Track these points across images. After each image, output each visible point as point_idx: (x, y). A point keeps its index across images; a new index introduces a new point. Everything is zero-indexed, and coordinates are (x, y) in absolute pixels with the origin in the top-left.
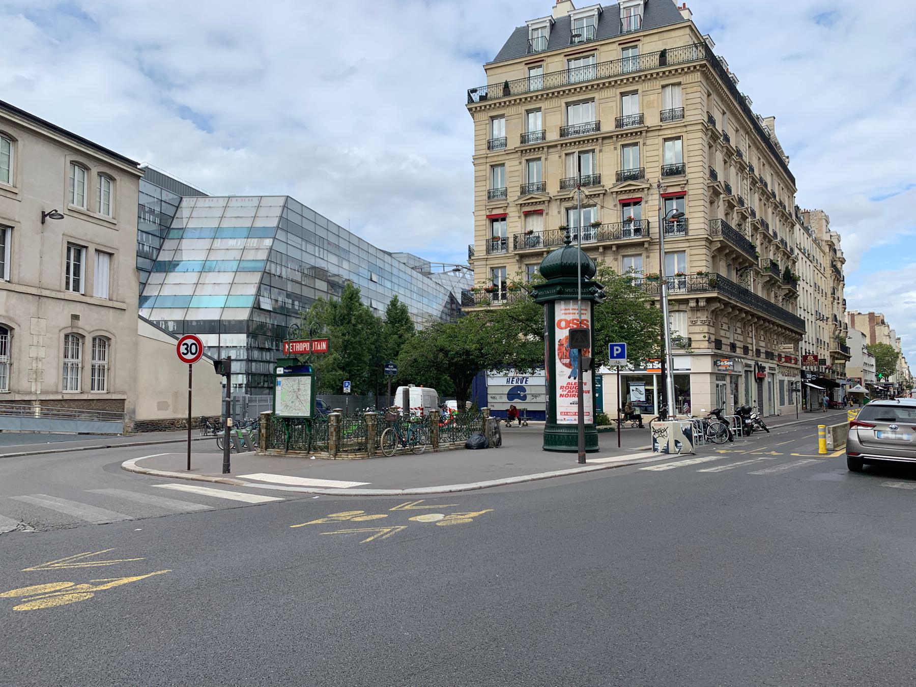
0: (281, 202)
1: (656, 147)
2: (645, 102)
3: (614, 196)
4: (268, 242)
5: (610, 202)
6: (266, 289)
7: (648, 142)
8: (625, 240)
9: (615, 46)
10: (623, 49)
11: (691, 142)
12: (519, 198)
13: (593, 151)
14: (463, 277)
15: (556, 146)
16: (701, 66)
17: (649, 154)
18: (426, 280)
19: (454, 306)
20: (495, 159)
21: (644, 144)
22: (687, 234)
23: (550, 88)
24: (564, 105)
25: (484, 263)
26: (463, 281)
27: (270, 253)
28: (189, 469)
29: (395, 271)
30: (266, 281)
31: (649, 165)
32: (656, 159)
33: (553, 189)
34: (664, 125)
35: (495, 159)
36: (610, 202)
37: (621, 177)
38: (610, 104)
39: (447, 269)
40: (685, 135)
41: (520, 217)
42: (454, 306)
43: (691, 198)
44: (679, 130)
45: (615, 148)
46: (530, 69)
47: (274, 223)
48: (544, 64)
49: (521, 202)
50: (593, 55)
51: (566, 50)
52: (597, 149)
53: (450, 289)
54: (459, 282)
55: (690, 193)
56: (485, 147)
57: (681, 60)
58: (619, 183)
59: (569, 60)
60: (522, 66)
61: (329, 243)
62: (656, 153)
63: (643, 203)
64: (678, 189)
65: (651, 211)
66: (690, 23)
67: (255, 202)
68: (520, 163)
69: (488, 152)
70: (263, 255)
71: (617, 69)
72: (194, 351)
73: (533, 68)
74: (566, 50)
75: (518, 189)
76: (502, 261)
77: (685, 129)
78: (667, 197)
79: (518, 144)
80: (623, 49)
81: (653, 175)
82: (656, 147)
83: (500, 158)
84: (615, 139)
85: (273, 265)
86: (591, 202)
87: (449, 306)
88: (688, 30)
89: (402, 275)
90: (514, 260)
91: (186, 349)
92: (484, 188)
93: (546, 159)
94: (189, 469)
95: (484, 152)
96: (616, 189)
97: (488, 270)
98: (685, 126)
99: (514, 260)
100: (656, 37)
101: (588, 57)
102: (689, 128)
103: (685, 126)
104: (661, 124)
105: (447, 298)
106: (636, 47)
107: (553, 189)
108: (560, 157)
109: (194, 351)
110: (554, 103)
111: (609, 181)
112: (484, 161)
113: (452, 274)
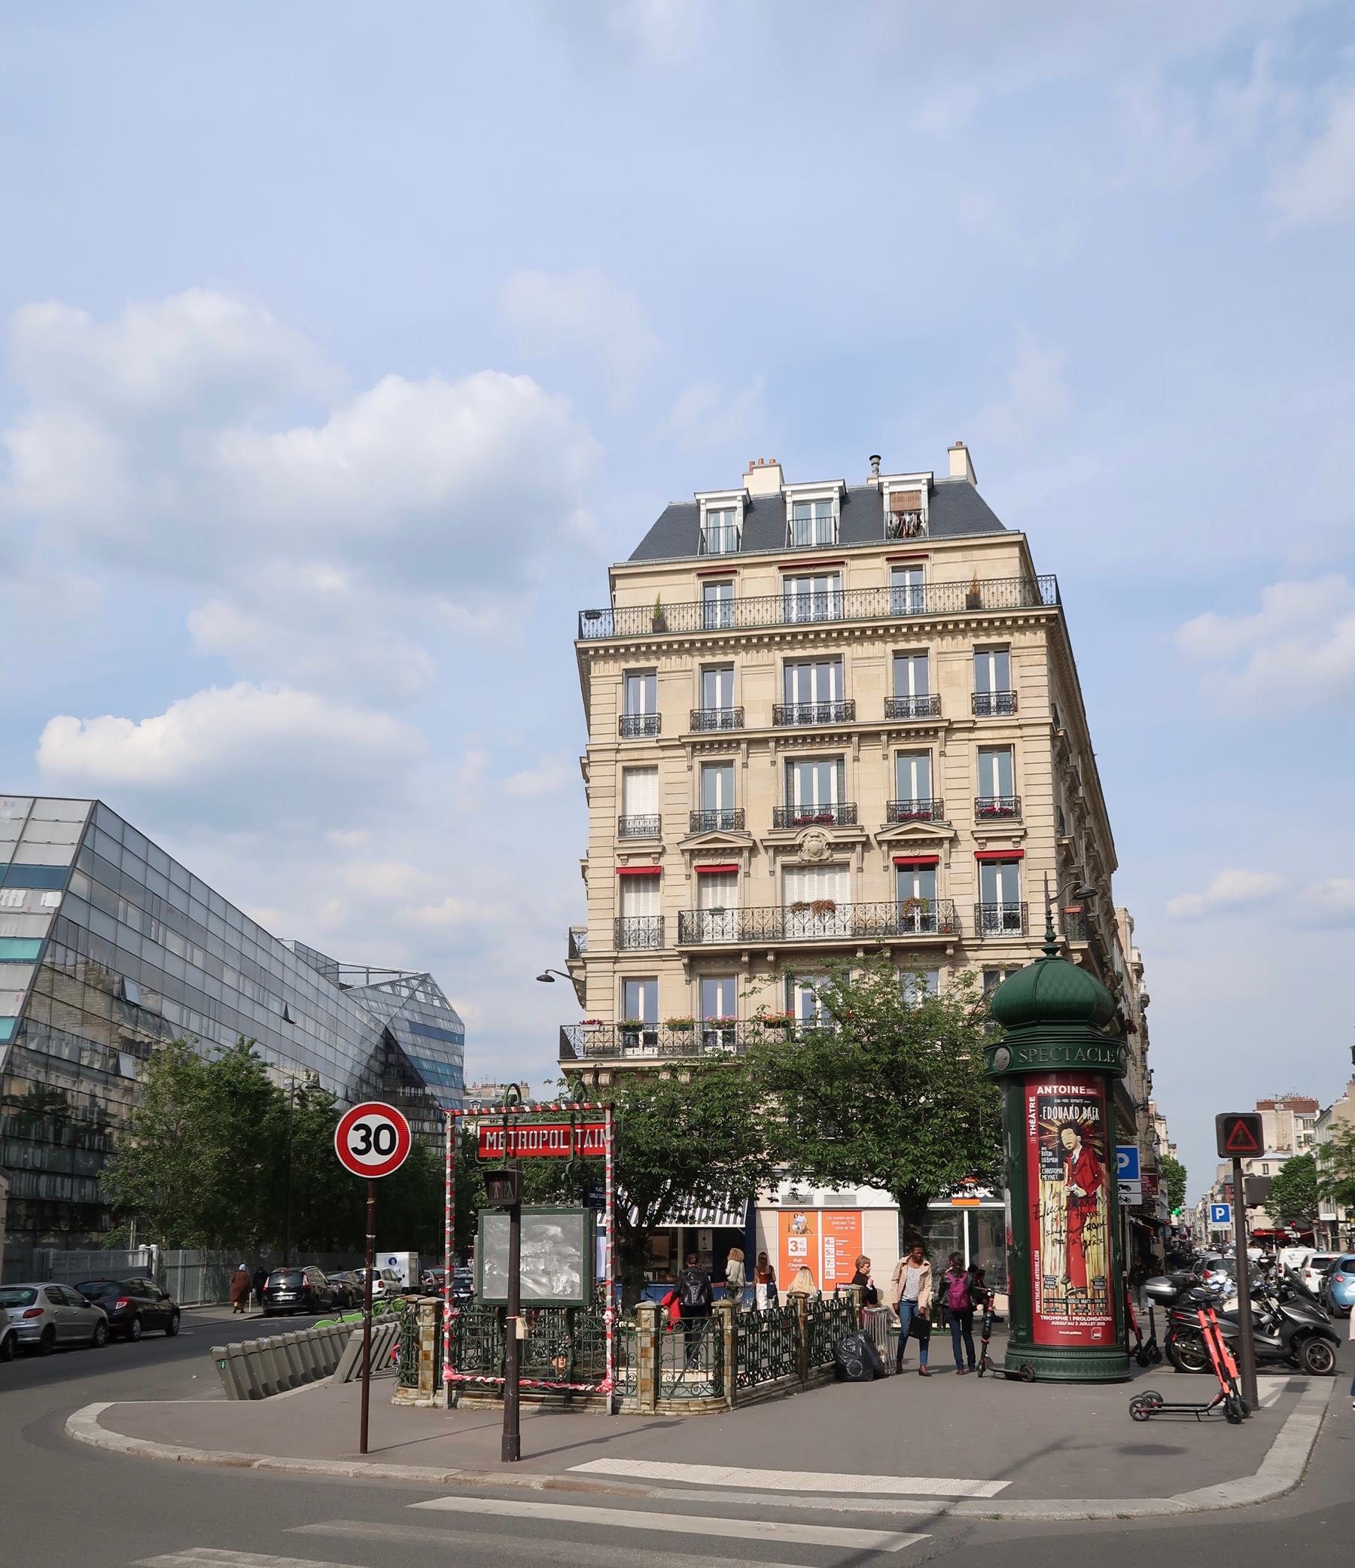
0: (83, 811)
1: (964, 761)
2: (942, 674)
3: (885, 848)
4: (52, 899)
5: (877, 859)
6: (42, 1004)
7: (949, 750)
8: (907, 938)
9: (881, 562)
10: (895, 570)
11: (1031, 758)
12: (688, 840)
13: (729, 763)
14: (411, 997)
15: (765, 741)
16: (1049, 618)
17: (951, 773)
18: (343, 1000)
19: (392, 1058)
20: (636, 755)
21: (942, 754)
22: (1025, 933)
23: (622, 638)
24: (780, 663)
25: (609, 966)
26: (412, 1005)
27: (54, 924)
28: (364, 1448)
29: (289, 978)
30: (42, 986)
31: (950, 794)
32: (965, 783)
33: (760, 825)
34: (982, 721)
35: (636, 755)
36: (877, 859)
37: (899, 814)
38: (873, 671)
39: (375, 979)
40: (1020, 746)
41: (688, 877)
42: (392, 1058)
43: (1032, 864)
44: (1007, 733)
45: (886, 757)
46: (787, 578)
47: (63, 857)
48: (736, 578)
49: (692, 845)
50: (836, 575)
51: (782, 558)
52: (739, 759)
53: (384, 1020)
54: (403, 1007)
55: (1030, 854)
56: (615, 728)
57: (1002, 603)
58: (894, 824)
59: (787, 578)
60: (881, 562)
61: (172, 909)
62: (963, 773)
63: (940, 869)
64: (1007, 846)
65: (958, 886)
66: (1020, 538)
67: (22, 808)
68: (690, 768)
69: (620, 739)
70: (40, 928)
71: (883, 605)
72: (385, 1144)
73: (713, 584)
74: (782, 558)
75: (686, 819)
76: (649, 965)
77: (1018, 732)
78: (986, 860)
79: (685, 730)
80: (895, 570)
81: (961, 816)
82: (964, 761)
83: (646, 754)
84: (772, 744)
85: (60, 950)
86: (839, 857)
87: (381, 1057)
88: (1015, 551)
89: (302, 987)
90: (679, 965)
91: (364, 1139)
92: (610, 812)
93: (745, 765)
94: (364, 1448)
95: (611, 739)
96: (888, 836)
97: (618, 983)
98: (1020, 727)
99: (679, 965)
100: (958, 556)
101: (824, 575)
102: (1027, 731)
103: (1020, 727)
104: (973, 717)
105: (376, 1039)
106: (919, 568)
107: (760, 825)
108: (774, 763)
109: (385, 1144)
110: (763, 656)
111: (873, 819)
112: (611, 756)
113: (387, 989)
